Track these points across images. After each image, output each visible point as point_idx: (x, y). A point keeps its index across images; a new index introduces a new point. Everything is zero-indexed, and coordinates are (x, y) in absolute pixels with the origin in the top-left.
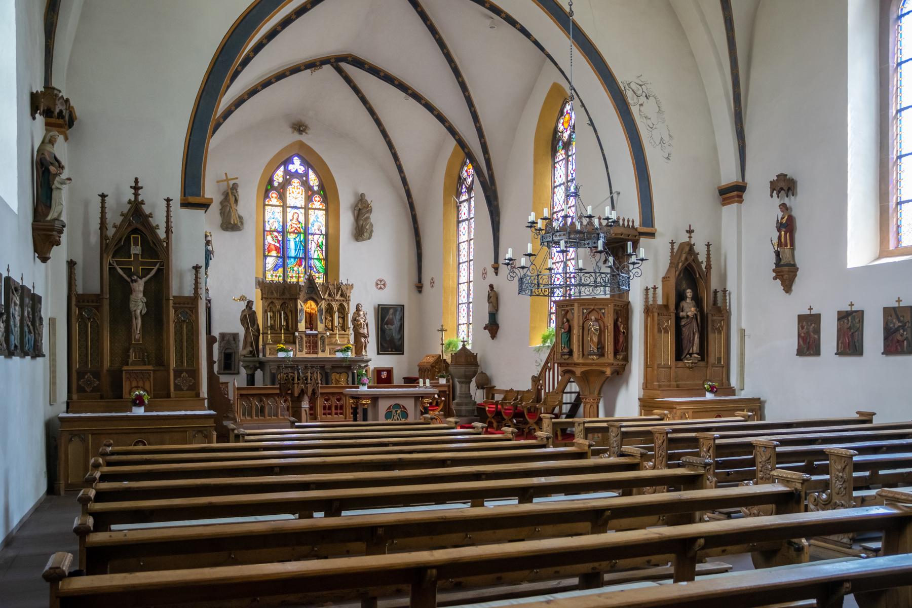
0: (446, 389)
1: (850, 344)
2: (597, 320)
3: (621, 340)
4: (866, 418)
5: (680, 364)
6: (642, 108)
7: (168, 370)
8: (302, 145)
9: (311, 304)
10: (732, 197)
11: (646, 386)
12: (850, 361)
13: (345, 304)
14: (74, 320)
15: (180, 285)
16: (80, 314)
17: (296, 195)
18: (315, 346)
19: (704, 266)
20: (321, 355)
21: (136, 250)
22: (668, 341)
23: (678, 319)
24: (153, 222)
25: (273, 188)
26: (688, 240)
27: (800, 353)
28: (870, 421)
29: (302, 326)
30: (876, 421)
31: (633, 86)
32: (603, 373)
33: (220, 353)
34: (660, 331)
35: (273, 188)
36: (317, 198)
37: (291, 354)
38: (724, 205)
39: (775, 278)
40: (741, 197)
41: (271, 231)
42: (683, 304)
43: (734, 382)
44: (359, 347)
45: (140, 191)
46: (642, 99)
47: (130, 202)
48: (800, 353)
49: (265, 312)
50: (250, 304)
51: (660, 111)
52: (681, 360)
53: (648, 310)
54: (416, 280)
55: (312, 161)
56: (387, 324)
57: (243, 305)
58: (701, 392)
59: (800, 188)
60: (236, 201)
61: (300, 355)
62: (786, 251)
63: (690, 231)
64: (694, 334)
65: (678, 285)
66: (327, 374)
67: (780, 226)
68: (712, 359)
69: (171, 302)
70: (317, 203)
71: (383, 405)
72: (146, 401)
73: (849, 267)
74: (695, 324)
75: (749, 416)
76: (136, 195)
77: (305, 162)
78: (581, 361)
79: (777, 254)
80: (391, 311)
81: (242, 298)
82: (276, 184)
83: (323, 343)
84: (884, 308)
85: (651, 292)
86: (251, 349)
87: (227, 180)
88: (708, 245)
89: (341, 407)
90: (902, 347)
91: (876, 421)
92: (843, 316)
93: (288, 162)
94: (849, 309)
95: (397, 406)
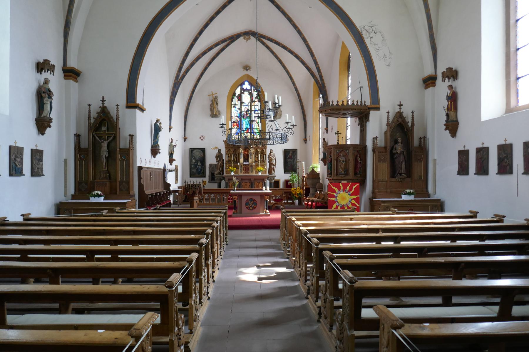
1: (505, 168)
2: (343, 156)
3: (358, 167)
5: (393, 179)
6: (372, 39)
7: (116, 182)
8: (248, 76)
10: (429, 84)
15: (123, 144)
19: (410, 124)
20: (250, 174)
21: (104, 128)
22: (385, 167)
23: (392, 155)
24: (112, 114)
26: (399, 110)
29: (242, 160)
31: (367, 28)
33: (209, 173)
39: (446, 129)
42: (396, 146)
43: (430, 190)
44: (271, 170)
45: (105, 102)
46: (372, 34)
47: (100, 107)
50: (220, 150)
51: (384, 39)
52: (395, 177)
53: (374, 150)
54: (304, 137)
55: (254, 84)
56: (289, 158)
57: (216, 152)
59: (460, 75)
60: (217, 104)
62: (452, 113)
63: (400, 105)
65: (391, 136)
68: (416, 176)
69: (118, 151)
71: (244, 199)
74: (402, 157)
76: (103, 104)
77: (250, 84)
79: (447, 115)
80: (291, 152)
81: (216, 148)
83: (252, 168)
85: (422, 140)
86: (219, 171)
87: (212, 95)
88: (413, 112)
89: (203, 199)
92: (479, 151)
93: (243, 84)
94: (481, 146)
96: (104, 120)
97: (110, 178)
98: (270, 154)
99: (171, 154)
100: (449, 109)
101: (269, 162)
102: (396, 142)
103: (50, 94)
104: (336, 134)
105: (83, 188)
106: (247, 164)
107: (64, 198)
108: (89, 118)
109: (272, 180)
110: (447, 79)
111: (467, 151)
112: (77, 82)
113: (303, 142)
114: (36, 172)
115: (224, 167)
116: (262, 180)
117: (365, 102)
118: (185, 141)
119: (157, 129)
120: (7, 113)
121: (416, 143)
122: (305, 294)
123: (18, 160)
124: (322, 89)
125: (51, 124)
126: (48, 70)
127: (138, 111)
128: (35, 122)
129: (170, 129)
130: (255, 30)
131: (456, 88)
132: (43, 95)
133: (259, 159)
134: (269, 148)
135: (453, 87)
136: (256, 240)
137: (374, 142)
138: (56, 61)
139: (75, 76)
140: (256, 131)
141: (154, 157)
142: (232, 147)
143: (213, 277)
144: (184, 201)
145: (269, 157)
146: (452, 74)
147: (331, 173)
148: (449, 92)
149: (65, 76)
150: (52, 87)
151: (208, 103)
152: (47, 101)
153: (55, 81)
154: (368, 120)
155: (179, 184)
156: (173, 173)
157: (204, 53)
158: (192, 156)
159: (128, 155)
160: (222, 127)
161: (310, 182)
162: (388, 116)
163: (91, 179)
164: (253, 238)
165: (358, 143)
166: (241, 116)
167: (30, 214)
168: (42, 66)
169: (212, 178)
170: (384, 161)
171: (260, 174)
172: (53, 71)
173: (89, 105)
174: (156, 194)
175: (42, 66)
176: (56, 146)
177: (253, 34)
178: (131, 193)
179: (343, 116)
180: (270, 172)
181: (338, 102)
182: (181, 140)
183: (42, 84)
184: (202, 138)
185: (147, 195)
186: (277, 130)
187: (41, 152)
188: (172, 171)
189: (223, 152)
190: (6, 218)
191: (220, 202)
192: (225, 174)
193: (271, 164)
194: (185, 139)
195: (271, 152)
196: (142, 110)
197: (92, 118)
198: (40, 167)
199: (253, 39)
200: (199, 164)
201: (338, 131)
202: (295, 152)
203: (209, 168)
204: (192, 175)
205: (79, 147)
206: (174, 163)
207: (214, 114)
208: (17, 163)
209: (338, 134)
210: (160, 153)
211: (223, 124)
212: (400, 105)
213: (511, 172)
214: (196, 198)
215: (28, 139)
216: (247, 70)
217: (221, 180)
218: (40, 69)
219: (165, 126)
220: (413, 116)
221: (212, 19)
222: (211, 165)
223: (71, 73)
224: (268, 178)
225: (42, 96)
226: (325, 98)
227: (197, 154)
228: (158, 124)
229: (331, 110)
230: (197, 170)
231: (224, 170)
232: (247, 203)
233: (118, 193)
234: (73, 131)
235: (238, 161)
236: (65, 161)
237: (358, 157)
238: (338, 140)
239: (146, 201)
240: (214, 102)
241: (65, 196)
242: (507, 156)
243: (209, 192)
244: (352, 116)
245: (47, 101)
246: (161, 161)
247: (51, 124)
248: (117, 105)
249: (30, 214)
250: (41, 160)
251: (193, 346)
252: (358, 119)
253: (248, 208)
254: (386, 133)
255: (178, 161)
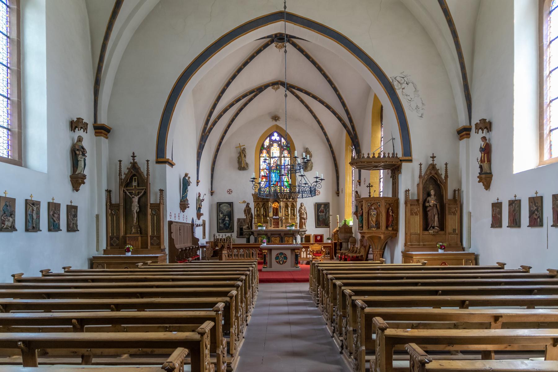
0: (331, 245)
3: (390, 220)
4: (502, 266)
5: (426, 233)
6: (404, 91)
7: (147, 237)
8: (277, 127)
9: (276, 204)
11: (405, 245)
12: (514, 230)
13: (294, 203)
14: (108, 215)
15: (153, 199)
16: (111, 213)
17: (275, 151)
18: (278, 224)
20: (280, 228)
21: (135, 184)
22: (418, 220)
23: (425, 208)
24: (142, 170)
25: (264, 148)
26: (431, 162)
27: (493, 226)
28: (503, 268)
29: (271, 214)
30: (506, 268)
31: (398, 79)
32: (380, 237)
34: (412, 214)
35: (264, 148)
36: (286, 152)
37: (264, 228)
38: (460, 140)
39: (479, 182)
40: (469, 134)
41: (263, 169)
42: (429, 198)
43: (465, 245)
44: (301, 225)
46: (404, 85)
47: (131, 163)
48: (493, 226)
49: (255, 208)
50: (248, 204)
51: (416, 90)
52: (428, 230)
53: (406, 203)
56: (320, 212)
57: (244, 206)
58: (435, 248)
59: (494, 127)
60: (245, 156)
61: (270, 228)
62: (485, 165)
63: (433, 157)
64: (434, 216)
65: (424, 188)
66: (282, 237)
67: (482, 150)
69: (149, 206)
70: (286, 153)
71: (274, 253)
72: (131, 250)
73: (515, 172)
74: (435, 210)
75: (425, 263)
76: (134, 160)
77: (279, 135)
78: (367, 231)
79: (481, 167)
80: (323, 206)
81: (244, 202)
82: (265, 146)
84: (529, 198)
85: (457, 192)
87: (240, 146)
88: (446, 164)
89: (231, 255)
90: (537, 222)
91: (506, 268)
92: (511, 203)
93: (272, 135)
94: (514, 199)
95: (282, 254)
96: (134, 175)
97: (141, 233)
98: (301, 208)
99: (199, 209)
100: (482, 161)
101: (300, 216)
102: (429, 195)
103: (83, 151)
104: (367, 186)
105: (116, 242)
106: (277, 219)
107: (96, 253)
108: (120, 174)
109: (303, 235)
110: (480, 130)
111: (501, 204)
112: (107, 138)
113: (336, 195)
114: (72, 228)
115: (253, 222)
116: (293, 234)
117: (397, 154)
118: (212, 195)
119: (185, 183)
120: (45, 170)
121: (450, 195)
122: (331, 334)
123: (56, 215)
124: (355, 141)
125: (85, 181)
126: (82, 128)
127: (168, 166)
128: (70, 179)
129: (198, 183)
130: (283, 79)
131: (489, 139)
132: (77, 153)
133: (289, 213)
134: (299, 201)
135: (487, 138)
136: (286, 292)
137: (406, 194)
138: (88, 119)
139: (106, 133)
140: (286, 184)
141: (183, 212)
142: (262, 200)
143: (246, 321)
144: (212, 256)
145: (299, 211)
146: (486, 125)
147: (362, 227)
148: (483, 143)
149: (96, 133)
150: (85, 144)
151: (235, 155)
152: (80, 157)
153: (88, 139)
154: (400, 173)
155: (207, 239)
156: (201, 228)
157: (231, 105)
158: (220, 211)
159: (159, 210)
160: (252, 181)
161: (341, 236)
162: (421, 168)
163: (122, 233)
164: (284, 290)
165: (390, 195)
166: (270, 169)
167: (71, 267)
168: (76, 125)
169: (241, 234)
170: (416, 214)
171: (294, 228)
172: (86, 129)
173: (120, 161)
174: (186, 249)
175: (76, 125)
176: (90, 202)
177: (283, 84)
178: (162, 247)
179: (374, 168)
180: (301, 226)
181: (368, 154)
182: (208, 194)
183: (76, 141)
184: (230, 192)
185: (178, 250)
186: (305, 184)
187: (76, 208)
188: (200, 226)
189: (252, 206)
190: (50, 270)
191: (250, 257)
192: (254, 228)
193: (301, 218)
194: (212, 193)
195: (301, 206)
196: (172, 165)
197: (123, 174)
198: (74, 222)
199: (282, 89)
200: (227, 219)
201: (370, 184)
202: (327, 205)
203: (238, 223)
204: (220, 230)
205: (110, 202)
206: (202, 218)
207: (242, 166)
208: (55, 219)
209: (370, 186)
210: (188, 207)
211: (254, 179)
212: (433, 157)
213: (541, 225)
214: (225, 252)
215: (64, 195)
216: (276, 120)
217: (250, 235)
218: (74, 127)
219: (193, 180)
220: (446, 168)
221: (239, 70)
222: (239, 220)
223: (102, 130)
224: (298, 232)
225: (76, 153)
226: (358, 152)
227: (225, 209)
228: (187, 178)
229: (363, 163)
230: (225, 225)
231: (253, 224)
232: (277, 258)
233: (149, 247)
234: (104, 187)
235: (266, 216)
236: (97, 216)
237: (390, 210)
238: (370, 193)
239: (178, 255)
240: (242, 153)
241: (97, 251)
242: (538, 209)
243: (238, 247)
244: (385, 168)
245: (81, 158)
246: (190, 214)
247: (85, 181)
248: (148, 161)
249: (71, 267)
250: (75, 216)
251: (235, 366)
252: (390, 171)
253: (279, 263)
254: (418, 185)
255: (205, 217)
